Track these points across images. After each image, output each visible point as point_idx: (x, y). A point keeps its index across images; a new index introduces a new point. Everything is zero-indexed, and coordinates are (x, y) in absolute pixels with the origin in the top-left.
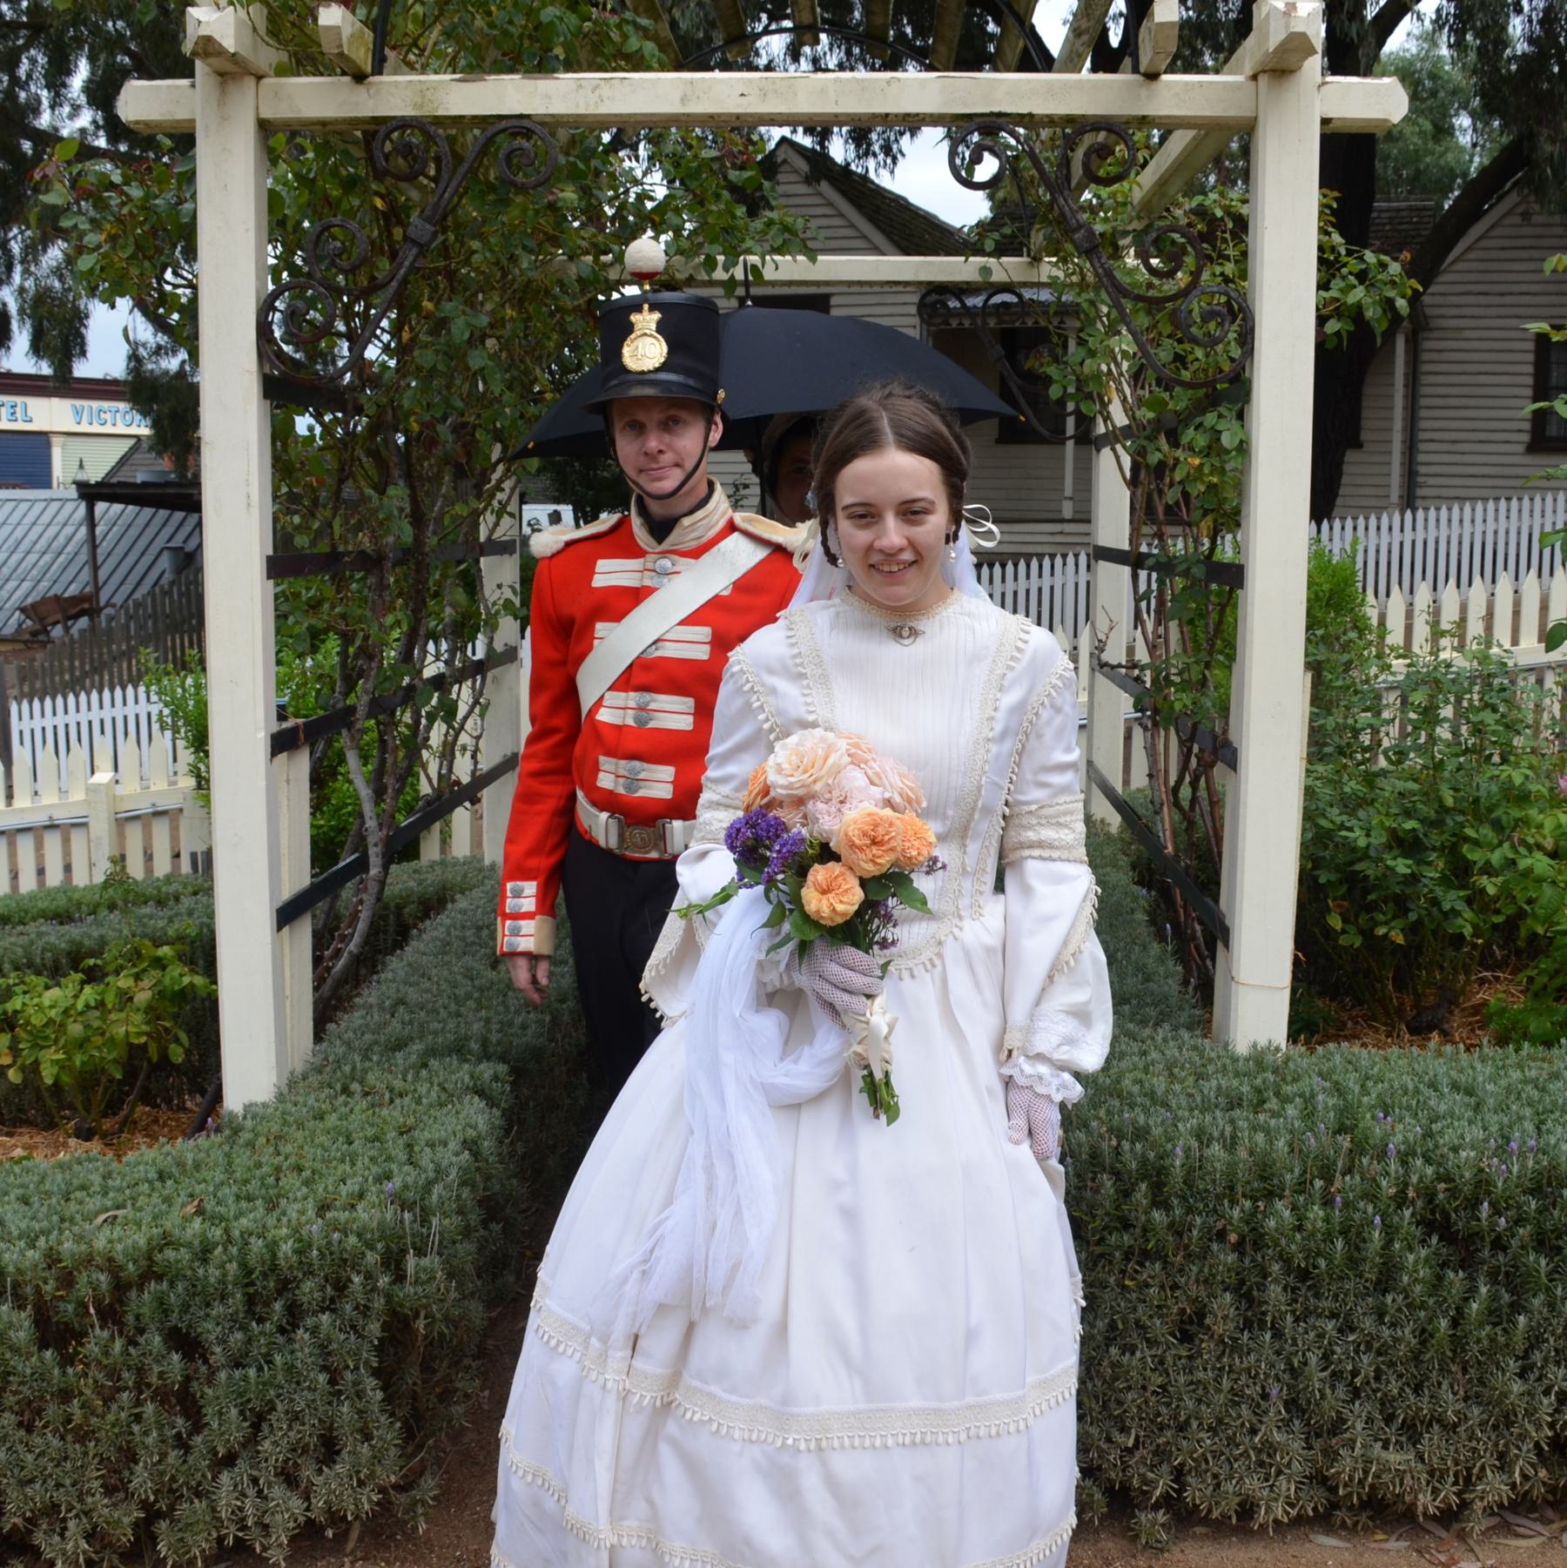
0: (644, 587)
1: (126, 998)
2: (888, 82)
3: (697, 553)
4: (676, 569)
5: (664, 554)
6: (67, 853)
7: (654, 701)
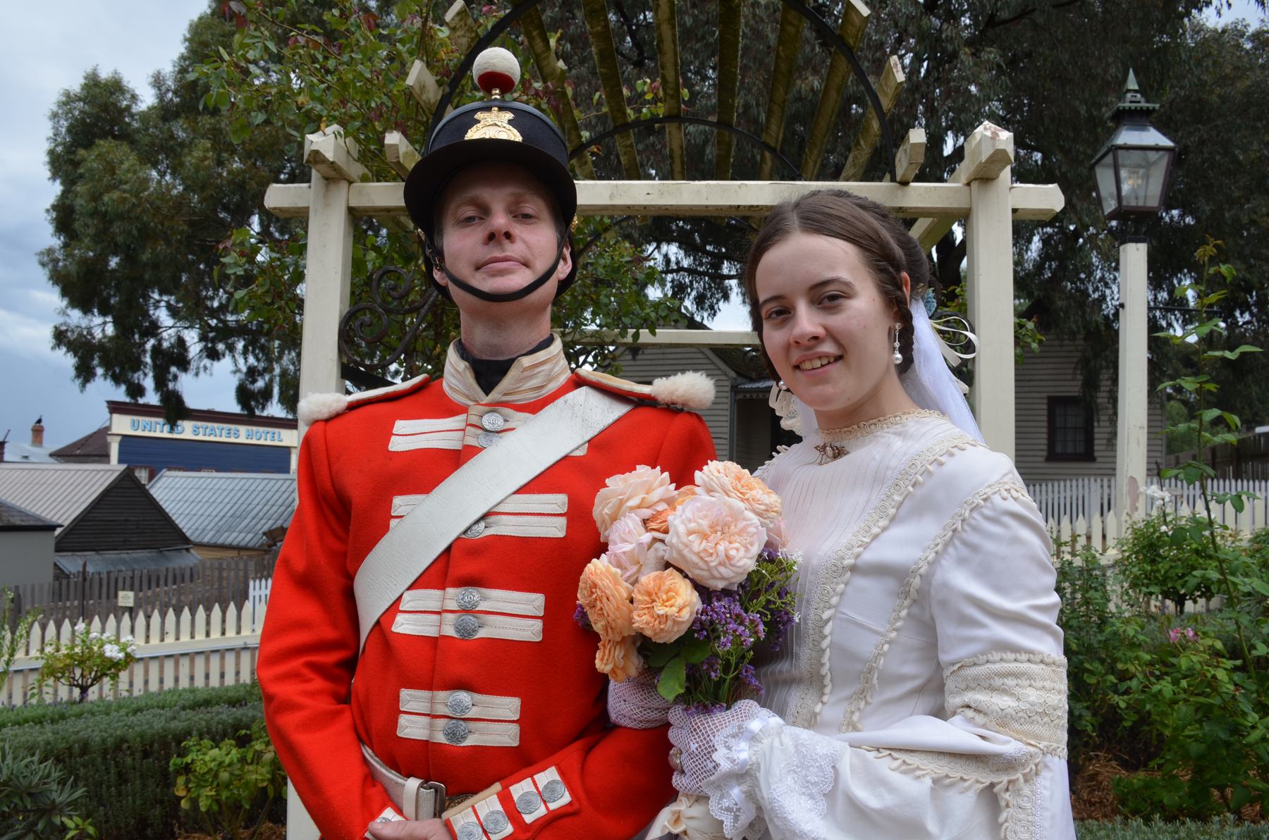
0: (467, 447)
1: (258, 755)
2: (739, 186)
3: (534, 407)
4: (509, 425)
5: (495, 406)
6: (238, 664)
7: (484, 598)
